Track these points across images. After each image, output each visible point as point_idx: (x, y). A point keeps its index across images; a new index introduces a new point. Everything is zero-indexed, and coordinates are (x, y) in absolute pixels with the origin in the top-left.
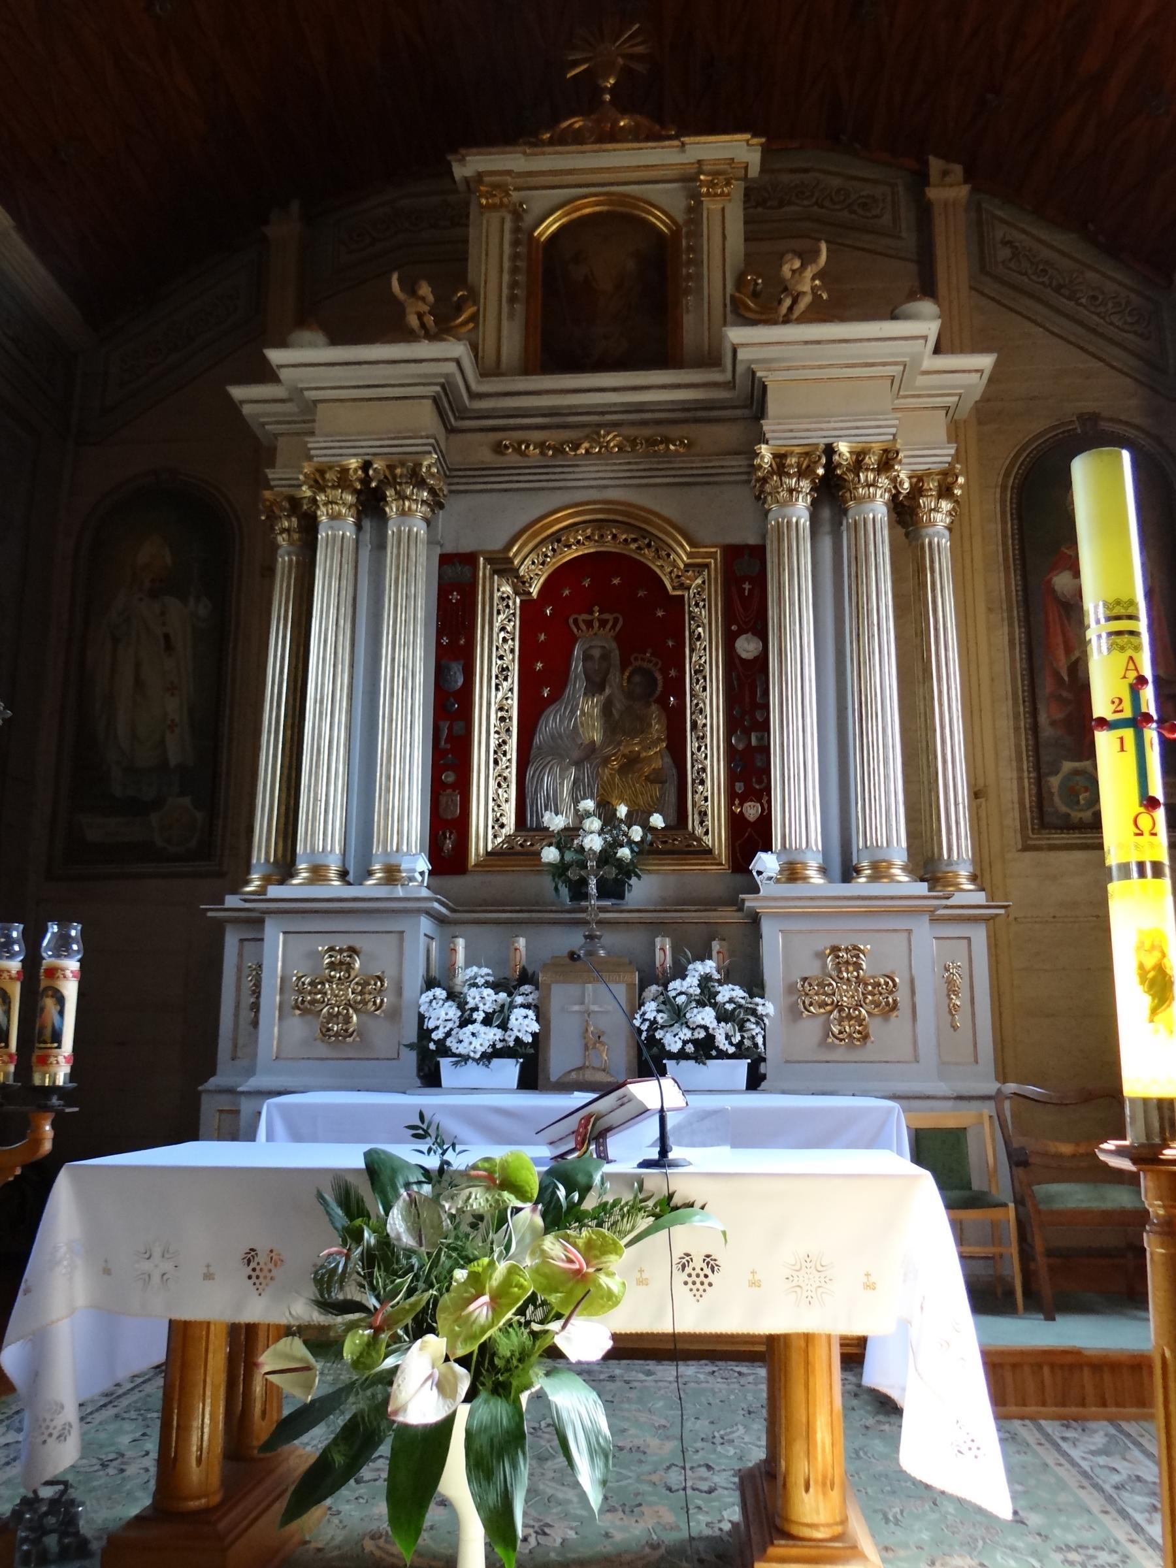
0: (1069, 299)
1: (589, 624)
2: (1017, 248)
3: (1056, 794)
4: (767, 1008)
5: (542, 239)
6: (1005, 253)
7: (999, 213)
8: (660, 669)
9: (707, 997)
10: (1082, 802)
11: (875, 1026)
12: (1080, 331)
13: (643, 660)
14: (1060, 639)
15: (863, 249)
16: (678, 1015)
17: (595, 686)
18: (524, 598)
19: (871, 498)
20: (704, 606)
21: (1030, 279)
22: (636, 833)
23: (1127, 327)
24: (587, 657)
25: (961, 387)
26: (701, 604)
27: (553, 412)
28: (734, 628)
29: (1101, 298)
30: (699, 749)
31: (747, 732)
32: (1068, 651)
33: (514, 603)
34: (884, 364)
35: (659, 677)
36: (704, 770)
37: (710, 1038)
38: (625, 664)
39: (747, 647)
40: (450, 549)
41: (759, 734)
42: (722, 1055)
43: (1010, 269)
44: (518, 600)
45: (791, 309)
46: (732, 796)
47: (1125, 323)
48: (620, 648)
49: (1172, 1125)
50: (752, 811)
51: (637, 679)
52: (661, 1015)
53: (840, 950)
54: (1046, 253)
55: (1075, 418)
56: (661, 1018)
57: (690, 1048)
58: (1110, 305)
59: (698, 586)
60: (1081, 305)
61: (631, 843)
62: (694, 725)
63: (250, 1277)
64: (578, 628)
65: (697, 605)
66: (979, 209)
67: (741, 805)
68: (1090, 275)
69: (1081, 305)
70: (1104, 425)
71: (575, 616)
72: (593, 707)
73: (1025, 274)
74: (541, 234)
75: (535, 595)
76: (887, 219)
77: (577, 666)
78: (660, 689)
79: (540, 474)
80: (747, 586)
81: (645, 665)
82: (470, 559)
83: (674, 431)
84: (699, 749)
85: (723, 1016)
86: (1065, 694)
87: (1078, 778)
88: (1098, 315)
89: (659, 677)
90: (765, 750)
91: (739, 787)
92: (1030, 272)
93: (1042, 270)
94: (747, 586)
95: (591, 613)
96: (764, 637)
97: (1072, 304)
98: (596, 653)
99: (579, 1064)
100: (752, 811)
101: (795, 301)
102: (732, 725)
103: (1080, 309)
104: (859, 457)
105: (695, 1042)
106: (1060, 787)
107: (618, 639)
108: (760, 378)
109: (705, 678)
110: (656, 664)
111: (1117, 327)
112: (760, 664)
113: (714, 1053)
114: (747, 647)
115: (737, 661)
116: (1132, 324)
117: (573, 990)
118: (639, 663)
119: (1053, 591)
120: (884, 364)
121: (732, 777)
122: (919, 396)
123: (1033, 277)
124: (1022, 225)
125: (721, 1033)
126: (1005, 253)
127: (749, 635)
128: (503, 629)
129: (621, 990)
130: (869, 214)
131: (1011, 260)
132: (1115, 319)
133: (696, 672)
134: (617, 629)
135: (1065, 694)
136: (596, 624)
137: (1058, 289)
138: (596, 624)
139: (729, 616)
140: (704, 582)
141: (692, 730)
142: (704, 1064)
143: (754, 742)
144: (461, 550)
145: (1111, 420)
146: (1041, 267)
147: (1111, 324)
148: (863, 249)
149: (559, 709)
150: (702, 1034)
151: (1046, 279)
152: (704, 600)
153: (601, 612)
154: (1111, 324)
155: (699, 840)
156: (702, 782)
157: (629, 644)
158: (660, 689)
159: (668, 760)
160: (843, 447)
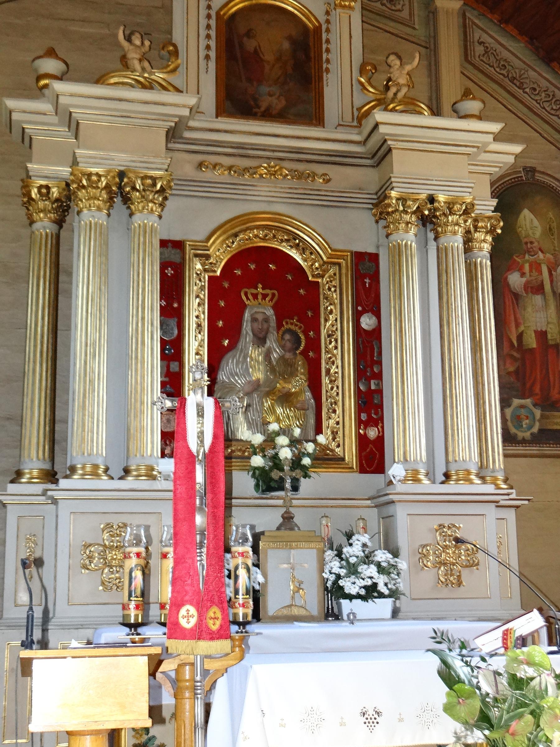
0: (519, 88)
1: (255, 296)
2: (487, 48)
3: (509, 420)
4: (403, 565)
5: (225, 17)
6: (480, 49)
7: (477, 21)
8: (303, 332)
9: (367, 559)
10: (524, 426)
11: (466, 574)
12: (525, 110)
13: (292, 324)
14: (512, 318)
15: (389, 32)
16: (353, 570)
17: (260, 340)
18: (211, 274)
19: (455, 233)
20: (335, 291)
21: (495, 69)
22: (310, 447)
23: (553, 112)
24: (254, 320)
25: (502, 163)
26: (333, 289)
27: (240, 146)
28: (360, 308)
29: (538, 89)
30: (332, 388)
31: (368, 380)
32: (517, 325)
33: (204, 278)
34: (466, 146)
35: (303, 337)
36: (336, 403)
37: (375, 585)
38: (279, 325)
39: (367, 322)
40: (165, 237)
41: (376, 382)
42: (381, 595)
43: (482, 60)
44: (207, 277)
45: (395, 94)
46: (359, 422)
47: (552, 109)
48: (276, 314)
49: (559, 632)
50: (372, 433)
51: (287, 337)
52: (342, 570)
53: (444, 527)
54: (505, 54)
55: (521, 170)
56: (343, 572)
57: (363, 592)
58: (543, 95)
59: (330, 277)
60: (526, 93)
61: (309, 455)
62: (328, 371)
63: (365, 723)
64: (248, 298)
65: (329, 289)
66: (464, 16)
67: (365, 428)
68: (532, 73)
69: (526, 93)
70: (538, 176)
71: (246, 290)
72: (259, 356)
73: (493, 66)
74: (224, 14)
75: (218, 273)
76: (405, 14)
77: (247, 327)
78: (303, 344)
79: (230, 188)
80: (367, 281)
81: (293, 327)
82: (179, 245)
83: (320, 169)
84: (332, 388)
85: (381, 570)
86: (515, 354)
87: (522, 410)
88: (536, 101)
89: (303, 337)
90: (380, 392)
91: (364, 417)
92: (495, 66)
93: (502, 65)
94: (367, 281)
95: (256, 288)
96: (378, 314)
97: (521, 91)
98: (260, 317)
99: (288, 603)
100: (372, 433)
101: (398, 91)
102: (360, 374)
103: (526, 95)
104: (450, 205)
105: (365, 587)
106: (512, 416)
107: (274, 307)
108: (389, 145)
109: (336, 340)
110: (300, 328)
111: (546, 110)
112: (376, 334)
113: (376, 594)
114: (367, 322)
115: (362, 332)
116: (556, 110)
117: (282, 553)
118: (290, 326)
119: (508, 285)
120: (466, 146)
121: (359, 410)
122: (477, 165)
123: (498, 70)
124: (491, 33)
125: (381, 580)
126: (480, 49)
127: (370, 314)
128: (197, 296)
129: (313, 553)
130: (393, 8)
131: (484, 55)
132: (546, 105)
133: (329, 336)
134: (274, 300)
135: (515, 354)
136: (260, 297)
137: (512, 80)
138: (260, 297)
139: (357, 301)
140: (335, 274)
141: (326, 376)
142: (368, 601)
143: (373, 387)
144: (171, 239)
145: (543, 173)
146: (502, 63)
147: (544, 108)
148: (389, 32)
149: (235, 356)
150: (369, 582)
151: (504, 72)
152: (335, 287)
153: (263, 289)
154: (544, 108)
155: (332, 451)
156: (334, 411)
157: (282, 313)
158: (303, 344)
159: (309, 394)
160: (442, 198)
